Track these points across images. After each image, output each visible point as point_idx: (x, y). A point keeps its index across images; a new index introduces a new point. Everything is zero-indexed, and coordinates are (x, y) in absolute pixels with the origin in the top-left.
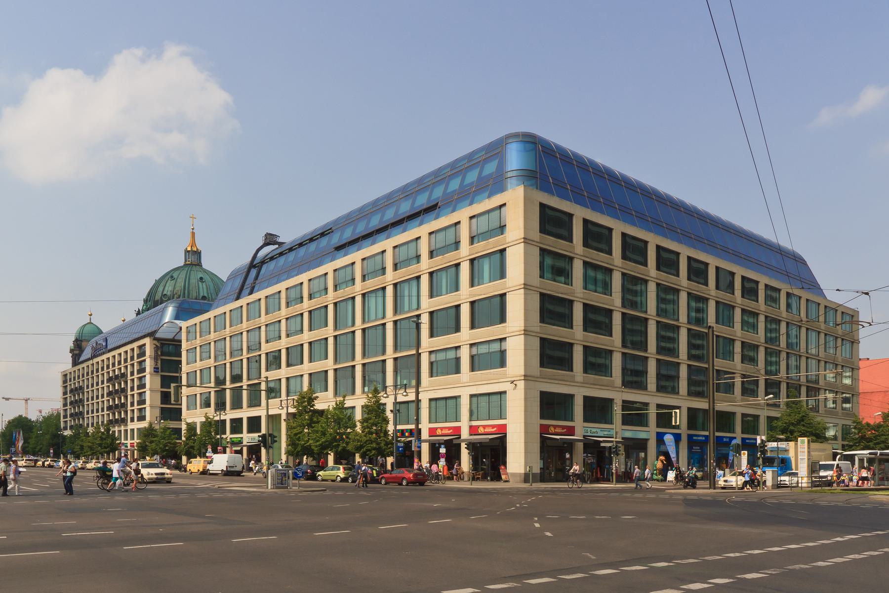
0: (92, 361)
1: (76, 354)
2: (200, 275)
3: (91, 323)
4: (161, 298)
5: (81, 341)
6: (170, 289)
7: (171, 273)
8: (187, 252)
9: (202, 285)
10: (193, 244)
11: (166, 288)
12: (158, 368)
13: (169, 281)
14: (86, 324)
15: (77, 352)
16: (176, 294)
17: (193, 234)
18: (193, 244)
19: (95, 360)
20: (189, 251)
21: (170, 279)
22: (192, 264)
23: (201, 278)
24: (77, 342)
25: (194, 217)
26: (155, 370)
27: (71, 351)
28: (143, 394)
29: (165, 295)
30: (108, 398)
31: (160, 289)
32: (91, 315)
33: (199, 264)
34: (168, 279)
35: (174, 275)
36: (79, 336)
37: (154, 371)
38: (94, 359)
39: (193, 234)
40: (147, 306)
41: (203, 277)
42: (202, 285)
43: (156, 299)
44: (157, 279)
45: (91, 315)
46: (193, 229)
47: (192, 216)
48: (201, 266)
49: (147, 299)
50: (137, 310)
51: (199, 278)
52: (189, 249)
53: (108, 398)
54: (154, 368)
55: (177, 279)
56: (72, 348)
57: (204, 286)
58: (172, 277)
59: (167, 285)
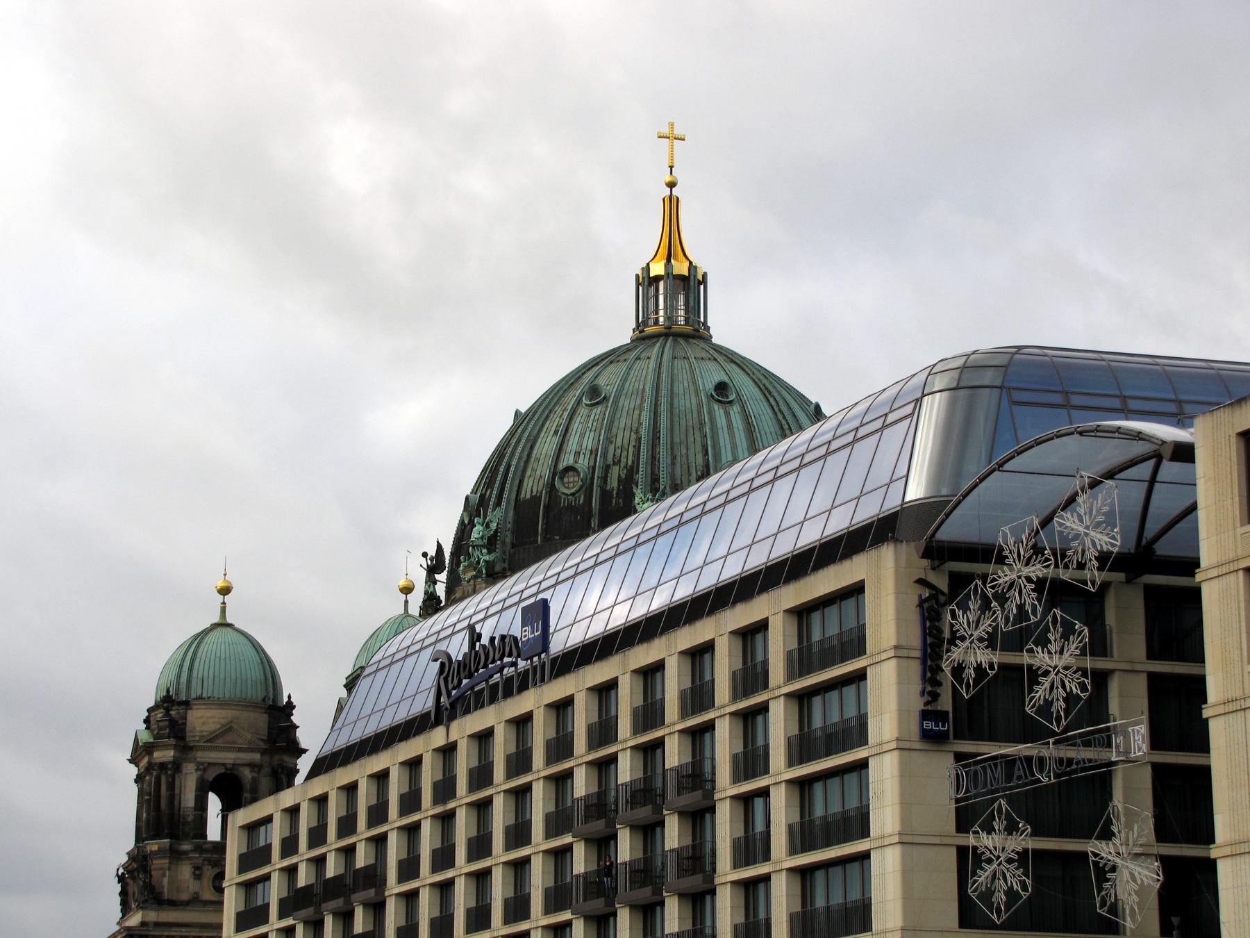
0: (440, 730)
1: (163, 766)
2: (712, 375)
3: (223, 624)
4: (551, 486)
5: (186, 704)
6: (589, 442)
7: (590, 374)
8: (647, 282)
9: (727, 414)
10: (672, 244)
11: (572, 444)
12: (941, 716)
13: (583, 411)
14: (205, 633)
15: (164, 755)
16: (617, 462)
17: (672, 206)
18: (672, 244)
19: (464, 728)
20: (657, 279)
21: (585, 401)
22: (669, 334)
23: (721, 388)
24: (167, 710)
25: (677, 132)
26: (929, 725)
27: (139, 752)
28: (761, 887)
29: (569, 469)
30: (289, 922)
31: (546, 446)
32: (225, 591)
33: (697, 333)
34: (579, 402)
35: (601, 381)
36: (178, 683)
37: (927, 736)
38: (455, 725)
39: (672, 206)
40: (488, 526)
41: (726, 379)
42: (727, 414)
43: (526, 494)
44: (523, 410)
45: (225, 591)
46: (671, 185)
47: (666, 131)
48: (707, 339)
49: (483, 501)
50: (432, 552)
51: (710, 386)
52: (658, 269)
53: (289, 922)
54: (925, 715)
55: (617, 398)
56: (145, 737)
57: (737, 421)
58: (594, 391)
59: (576, 425)
